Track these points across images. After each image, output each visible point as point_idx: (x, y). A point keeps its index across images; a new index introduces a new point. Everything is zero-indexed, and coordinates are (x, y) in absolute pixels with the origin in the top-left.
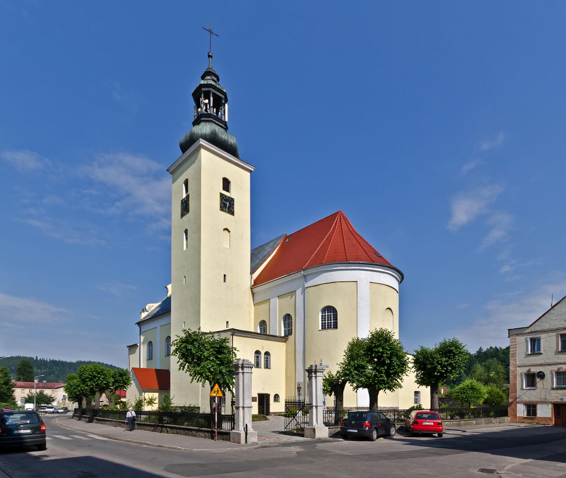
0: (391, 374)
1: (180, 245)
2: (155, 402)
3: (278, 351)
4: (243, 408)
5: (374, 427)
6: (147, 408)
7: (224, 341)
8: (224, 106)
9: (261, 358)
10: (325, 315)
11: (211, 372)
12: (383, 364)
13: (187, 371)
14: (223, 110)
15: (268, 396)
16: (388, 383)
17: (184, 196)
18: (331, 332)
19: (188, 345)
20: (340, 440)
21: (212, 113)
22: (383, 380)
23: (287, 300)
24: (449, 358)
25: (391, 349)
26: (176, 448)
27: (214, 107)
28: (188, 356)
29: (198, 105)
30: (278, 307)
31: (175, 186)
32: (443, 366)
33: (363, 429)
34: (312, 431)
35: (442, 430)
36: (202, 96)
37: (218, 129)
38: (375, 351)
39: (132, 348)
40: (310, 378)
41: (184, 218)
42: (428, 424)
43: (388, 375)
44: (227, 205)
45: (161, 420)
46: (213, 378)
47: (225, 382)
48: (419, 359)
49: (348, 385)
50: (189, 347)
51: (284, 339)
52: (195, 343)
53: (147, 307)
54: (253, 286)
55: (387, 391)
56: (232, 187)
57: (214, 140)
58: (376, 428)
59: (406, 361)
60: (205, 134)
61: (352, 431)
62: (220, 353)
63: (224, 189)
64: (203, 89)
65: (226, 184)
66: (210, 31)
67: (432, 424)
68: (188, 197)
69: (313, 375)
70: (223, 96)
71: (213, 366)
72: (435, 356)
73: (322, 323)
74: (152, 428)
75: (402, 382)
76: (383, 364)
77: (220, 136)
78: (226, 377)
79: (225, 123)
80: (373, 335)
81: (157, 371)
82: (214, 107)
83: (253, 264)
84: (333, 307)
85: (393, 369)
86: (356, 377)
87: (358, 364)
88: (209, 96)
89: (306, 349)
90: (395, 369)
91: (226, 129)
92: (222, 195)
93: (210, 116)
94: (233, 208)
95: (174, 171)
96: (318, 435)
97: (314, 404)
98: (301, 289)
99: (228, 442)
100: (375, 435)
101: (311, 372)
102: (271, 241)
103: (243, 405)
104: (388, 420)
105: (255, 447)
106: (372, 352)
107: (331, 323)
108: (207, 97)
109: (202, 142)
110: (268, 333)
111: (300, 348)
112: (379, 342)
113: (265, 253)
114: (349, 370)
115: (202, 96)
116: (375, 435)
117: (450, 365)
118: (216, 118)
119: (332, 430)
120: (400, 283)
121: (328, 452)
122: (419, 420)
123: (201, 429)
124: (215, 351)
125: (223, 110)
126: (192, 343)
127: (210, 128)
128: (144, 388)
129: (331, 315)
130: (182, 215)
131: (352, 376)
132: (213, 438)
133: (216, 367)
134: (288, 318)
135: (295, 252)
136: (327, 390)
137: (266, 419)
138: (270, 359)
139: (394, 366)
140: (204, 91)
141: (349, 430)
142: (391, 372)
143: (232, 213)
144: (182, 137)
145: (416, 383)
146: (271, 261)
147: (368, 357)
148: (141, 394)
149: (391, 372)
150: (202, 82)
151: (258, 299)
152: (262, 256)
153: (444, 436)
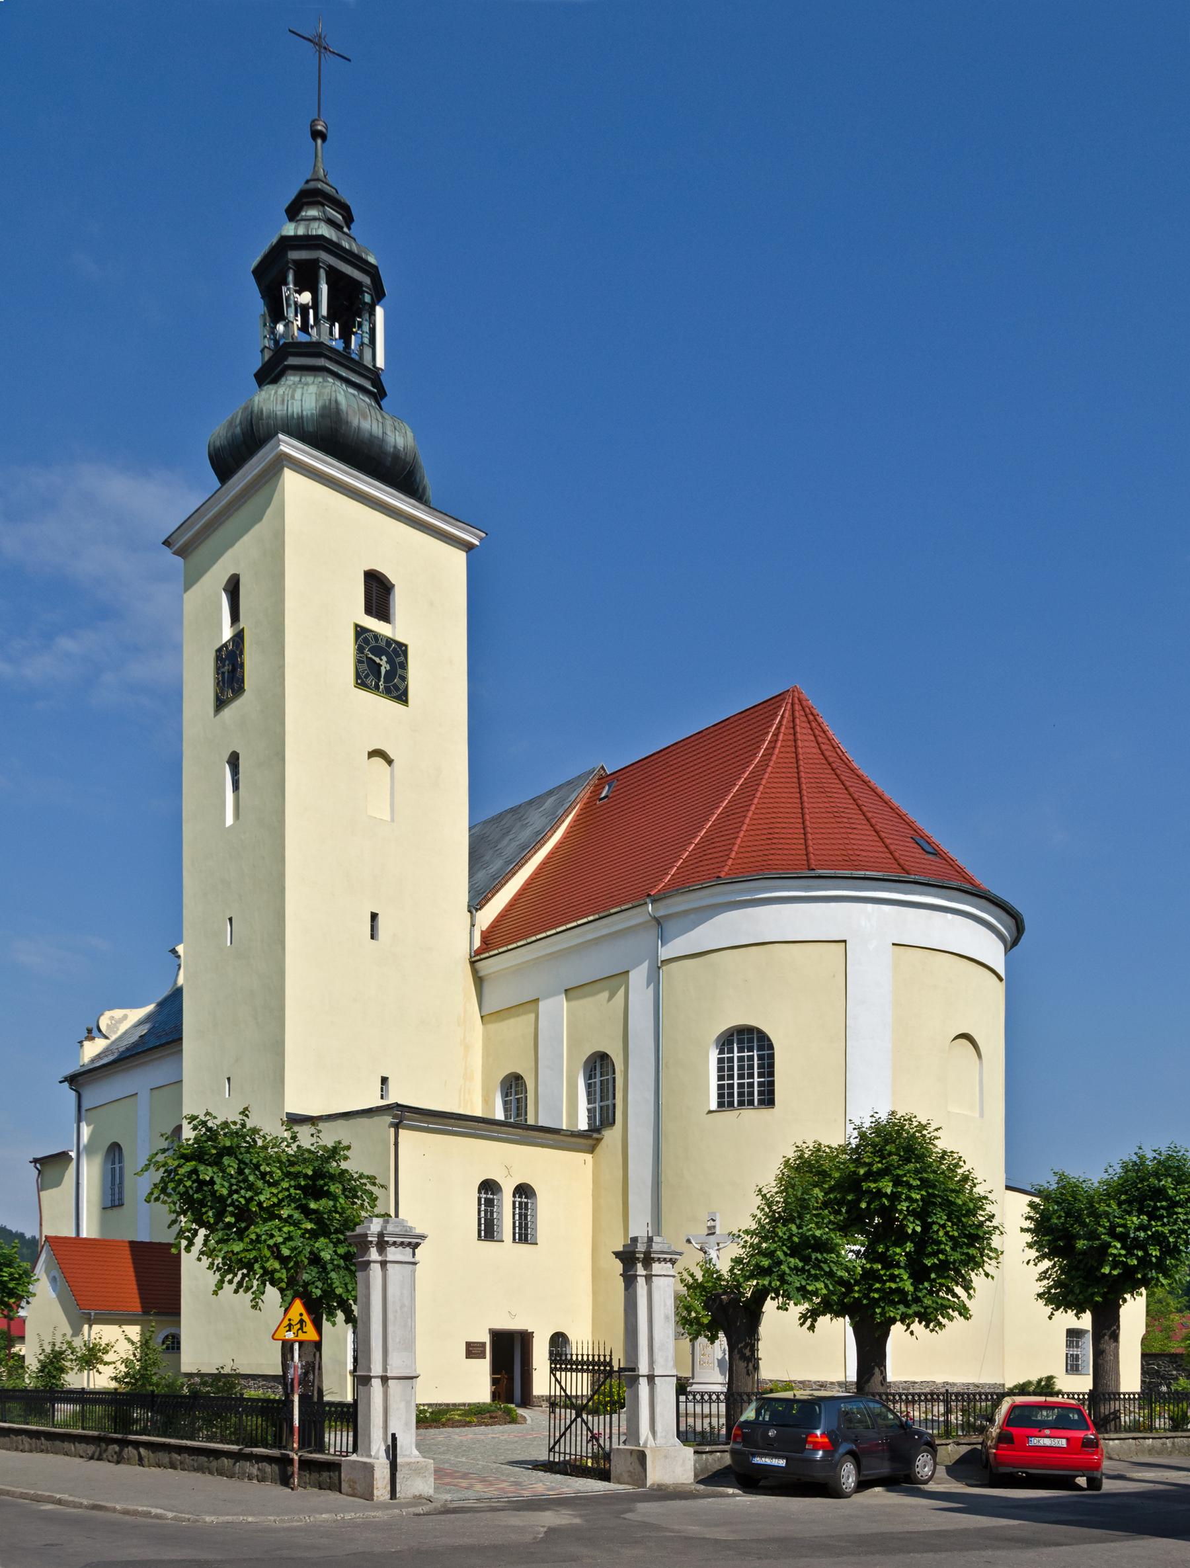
0: (928, 1270)
1: (211, 808)
2: (106, 1358)
3: (566, 1186)
4: (385, 1379)
5: (843, 1448)
6: (75, 1380)
7: (335, 1152)
8: (372, 313)
9: (500, 1206)
10: (731, 1060)
11: (283, 1260)
12: (902, 1237)
13: (202, 1253)
14: (366, 328)
15: (524, 1339)
16: (917, 1300)
17: (227, 634)
18: (751, 1117)
19: (201, 1168)
20: (730, 1491)
21: (325, 339)
22: (900, 1291)
23: (597, 1006)
24: (1152, 1216)
25: (925, 1184)
26: (147, 1514)
27: (332, 318)
28: (202, 1203)
29: (276, 312)
30: (564, 1031)
31: (192, 599)
32: (1131, 1245)
33: (805, 1454)
34: (634, 1458)
35: (1097, 1466)
36: (291, 278)
37: (345, 397)
38: (869, 1191)
39: (51, 1166)
40: (629, 1280)
41: (227, 712)
42: (1047, 1442)
43: (919, 1274)
44: (382, 667)
45: (123, 1422)
46: (292, 1281)
47: (329, 1293)
48: (1049, 1219)
49: (770, 1306)
50: (207, 1173)
51: (589, 1140)
52: (226, 1160)
53: (104, 1023)
54: (478, 952)
55: (917, 1327)
56: (400, 602)
57: (331, 437)
58: (851, 1453)
59: (981, 1224)
60: (301, 417)
61: (767, 1461)
62: (319, 1193)
63: (368, 611)
64: (294, 255)
65: (379, 593)
66: (319, 44)
67: (1063, 1443)
68: (238, 638)
69: (640, 1270)
70: (366, 280)
71: (289, 1238)
72: (1102, 1208)
73: (720, 1087)
74: (91, 1449)
75: (970, 1296)
76: (902, 1237)
77: (355, 422)
78: (333, 1275)
79: (374, 375)
80: (862, 1136)
81: (139, 1250)
82: (332, 318)
83: (481, 875)
84: (760, 1032)
85: (935, 1254)
86: (797, 1281)
87: (802, 1236)
88: (318, 280)
89: (663, 1178)
90: (943, 1252)
91: (378, 394)
92: (360, 631)
93: (316, 349)
94: (404, 679)
95: (191, 543)
96: (656, 1474)
97: (643, 1369)
98: (644, 967)
99: (332, 1496)
100: (848, 1476)
101: (633, 1260)
102: (550, 793)
103: (385, 1369)
104: (904, 1426)
105: (419, 1510)
106: (861, 1194)
107: (751, 1085)
108: (307, 282)
109: (288, 446)
110: (531, 1121)
111: (641, 1172)
112: (883, 1157)
113: (525, 835)
114: (770, 1254)
115: (291, 278)
116: (848, 1476)
117: (1158, 1239)
118: (344, 358)
119: (710, 1457)
120: (1011, 945)
121: (658, 1528)
122: (1014, 1431)
123: (248, 1450)
124: (298, 1187)
125: (366, 328)
126: (217, 1162)
127: (319, 395)
128: (86, 1307)
129: (751, 1058)
130: (220, 704)
131: (782, 1278)
132: (285, 1481)
133: (298, 1243)
134: (599, 1068)
135: (627, 838)
136: (699, 1324)
137: (513, 1421)
138: (534, 1210)
139: (939, 1243)
140: (295, 262)
141: (757, 1460)
142: (928, 1262)
143: (402, 697)
144: (218, 428)
145: (1041, 1302)
146: (544, 864)
147: (838, 1212)
148: (77, 1332)
149: (928, 1262)
150: (290, 229)
151: (497, 998)
152: (514, 844)
153: (1108, 1486)
